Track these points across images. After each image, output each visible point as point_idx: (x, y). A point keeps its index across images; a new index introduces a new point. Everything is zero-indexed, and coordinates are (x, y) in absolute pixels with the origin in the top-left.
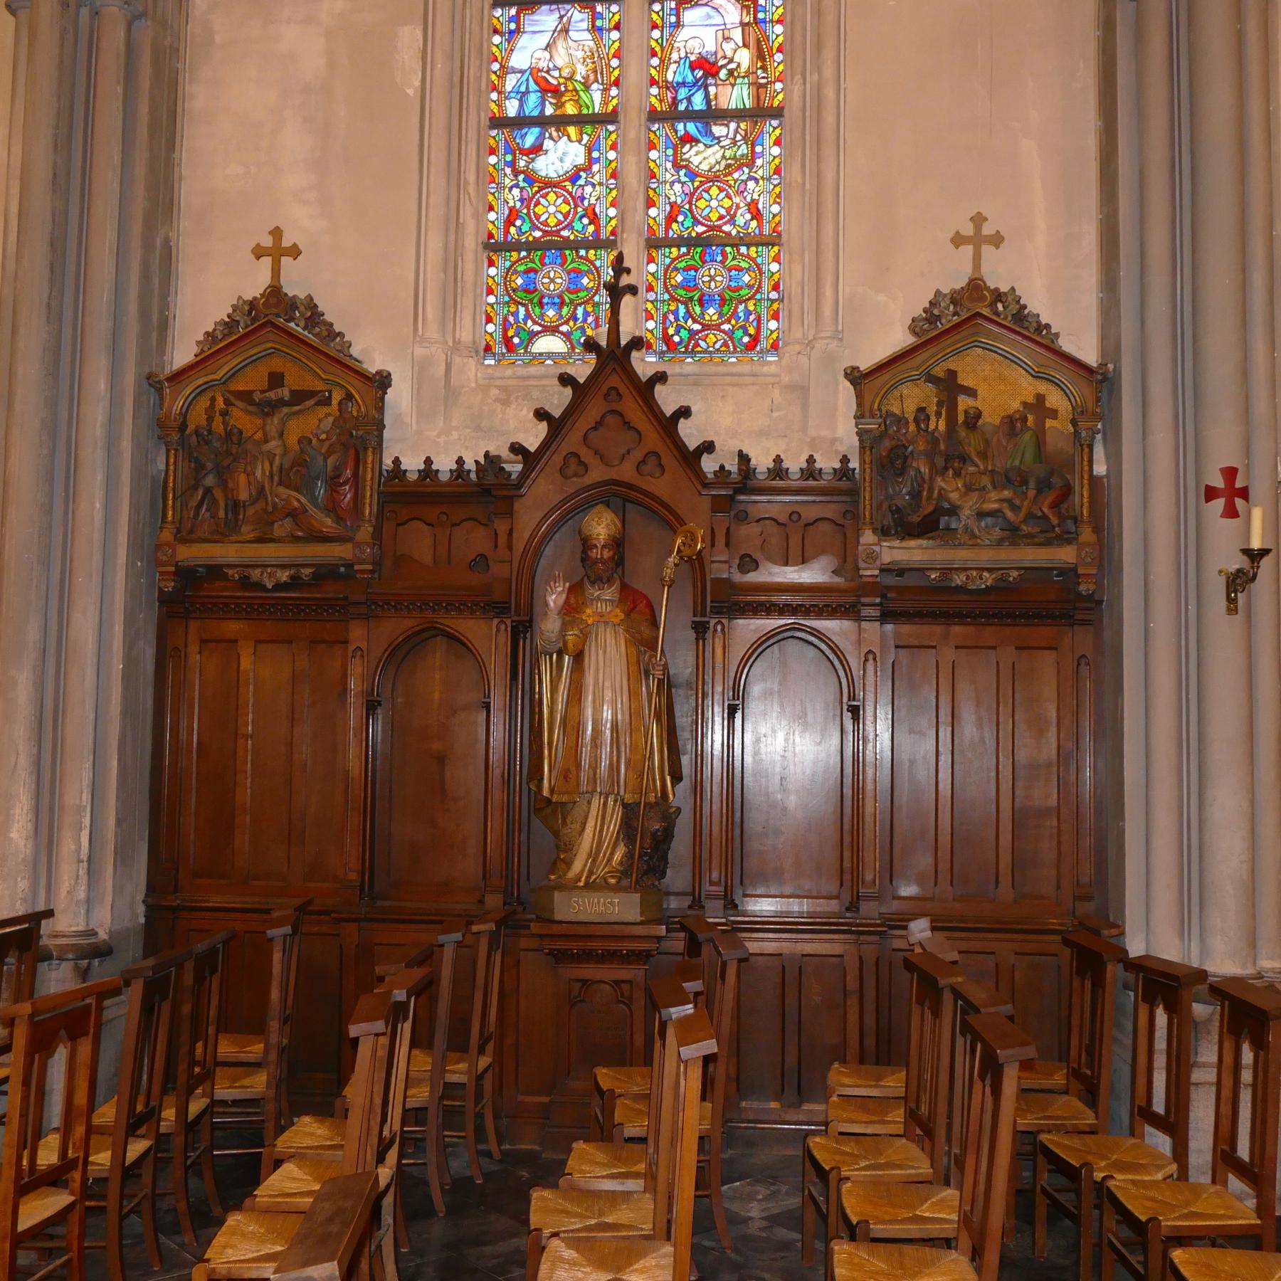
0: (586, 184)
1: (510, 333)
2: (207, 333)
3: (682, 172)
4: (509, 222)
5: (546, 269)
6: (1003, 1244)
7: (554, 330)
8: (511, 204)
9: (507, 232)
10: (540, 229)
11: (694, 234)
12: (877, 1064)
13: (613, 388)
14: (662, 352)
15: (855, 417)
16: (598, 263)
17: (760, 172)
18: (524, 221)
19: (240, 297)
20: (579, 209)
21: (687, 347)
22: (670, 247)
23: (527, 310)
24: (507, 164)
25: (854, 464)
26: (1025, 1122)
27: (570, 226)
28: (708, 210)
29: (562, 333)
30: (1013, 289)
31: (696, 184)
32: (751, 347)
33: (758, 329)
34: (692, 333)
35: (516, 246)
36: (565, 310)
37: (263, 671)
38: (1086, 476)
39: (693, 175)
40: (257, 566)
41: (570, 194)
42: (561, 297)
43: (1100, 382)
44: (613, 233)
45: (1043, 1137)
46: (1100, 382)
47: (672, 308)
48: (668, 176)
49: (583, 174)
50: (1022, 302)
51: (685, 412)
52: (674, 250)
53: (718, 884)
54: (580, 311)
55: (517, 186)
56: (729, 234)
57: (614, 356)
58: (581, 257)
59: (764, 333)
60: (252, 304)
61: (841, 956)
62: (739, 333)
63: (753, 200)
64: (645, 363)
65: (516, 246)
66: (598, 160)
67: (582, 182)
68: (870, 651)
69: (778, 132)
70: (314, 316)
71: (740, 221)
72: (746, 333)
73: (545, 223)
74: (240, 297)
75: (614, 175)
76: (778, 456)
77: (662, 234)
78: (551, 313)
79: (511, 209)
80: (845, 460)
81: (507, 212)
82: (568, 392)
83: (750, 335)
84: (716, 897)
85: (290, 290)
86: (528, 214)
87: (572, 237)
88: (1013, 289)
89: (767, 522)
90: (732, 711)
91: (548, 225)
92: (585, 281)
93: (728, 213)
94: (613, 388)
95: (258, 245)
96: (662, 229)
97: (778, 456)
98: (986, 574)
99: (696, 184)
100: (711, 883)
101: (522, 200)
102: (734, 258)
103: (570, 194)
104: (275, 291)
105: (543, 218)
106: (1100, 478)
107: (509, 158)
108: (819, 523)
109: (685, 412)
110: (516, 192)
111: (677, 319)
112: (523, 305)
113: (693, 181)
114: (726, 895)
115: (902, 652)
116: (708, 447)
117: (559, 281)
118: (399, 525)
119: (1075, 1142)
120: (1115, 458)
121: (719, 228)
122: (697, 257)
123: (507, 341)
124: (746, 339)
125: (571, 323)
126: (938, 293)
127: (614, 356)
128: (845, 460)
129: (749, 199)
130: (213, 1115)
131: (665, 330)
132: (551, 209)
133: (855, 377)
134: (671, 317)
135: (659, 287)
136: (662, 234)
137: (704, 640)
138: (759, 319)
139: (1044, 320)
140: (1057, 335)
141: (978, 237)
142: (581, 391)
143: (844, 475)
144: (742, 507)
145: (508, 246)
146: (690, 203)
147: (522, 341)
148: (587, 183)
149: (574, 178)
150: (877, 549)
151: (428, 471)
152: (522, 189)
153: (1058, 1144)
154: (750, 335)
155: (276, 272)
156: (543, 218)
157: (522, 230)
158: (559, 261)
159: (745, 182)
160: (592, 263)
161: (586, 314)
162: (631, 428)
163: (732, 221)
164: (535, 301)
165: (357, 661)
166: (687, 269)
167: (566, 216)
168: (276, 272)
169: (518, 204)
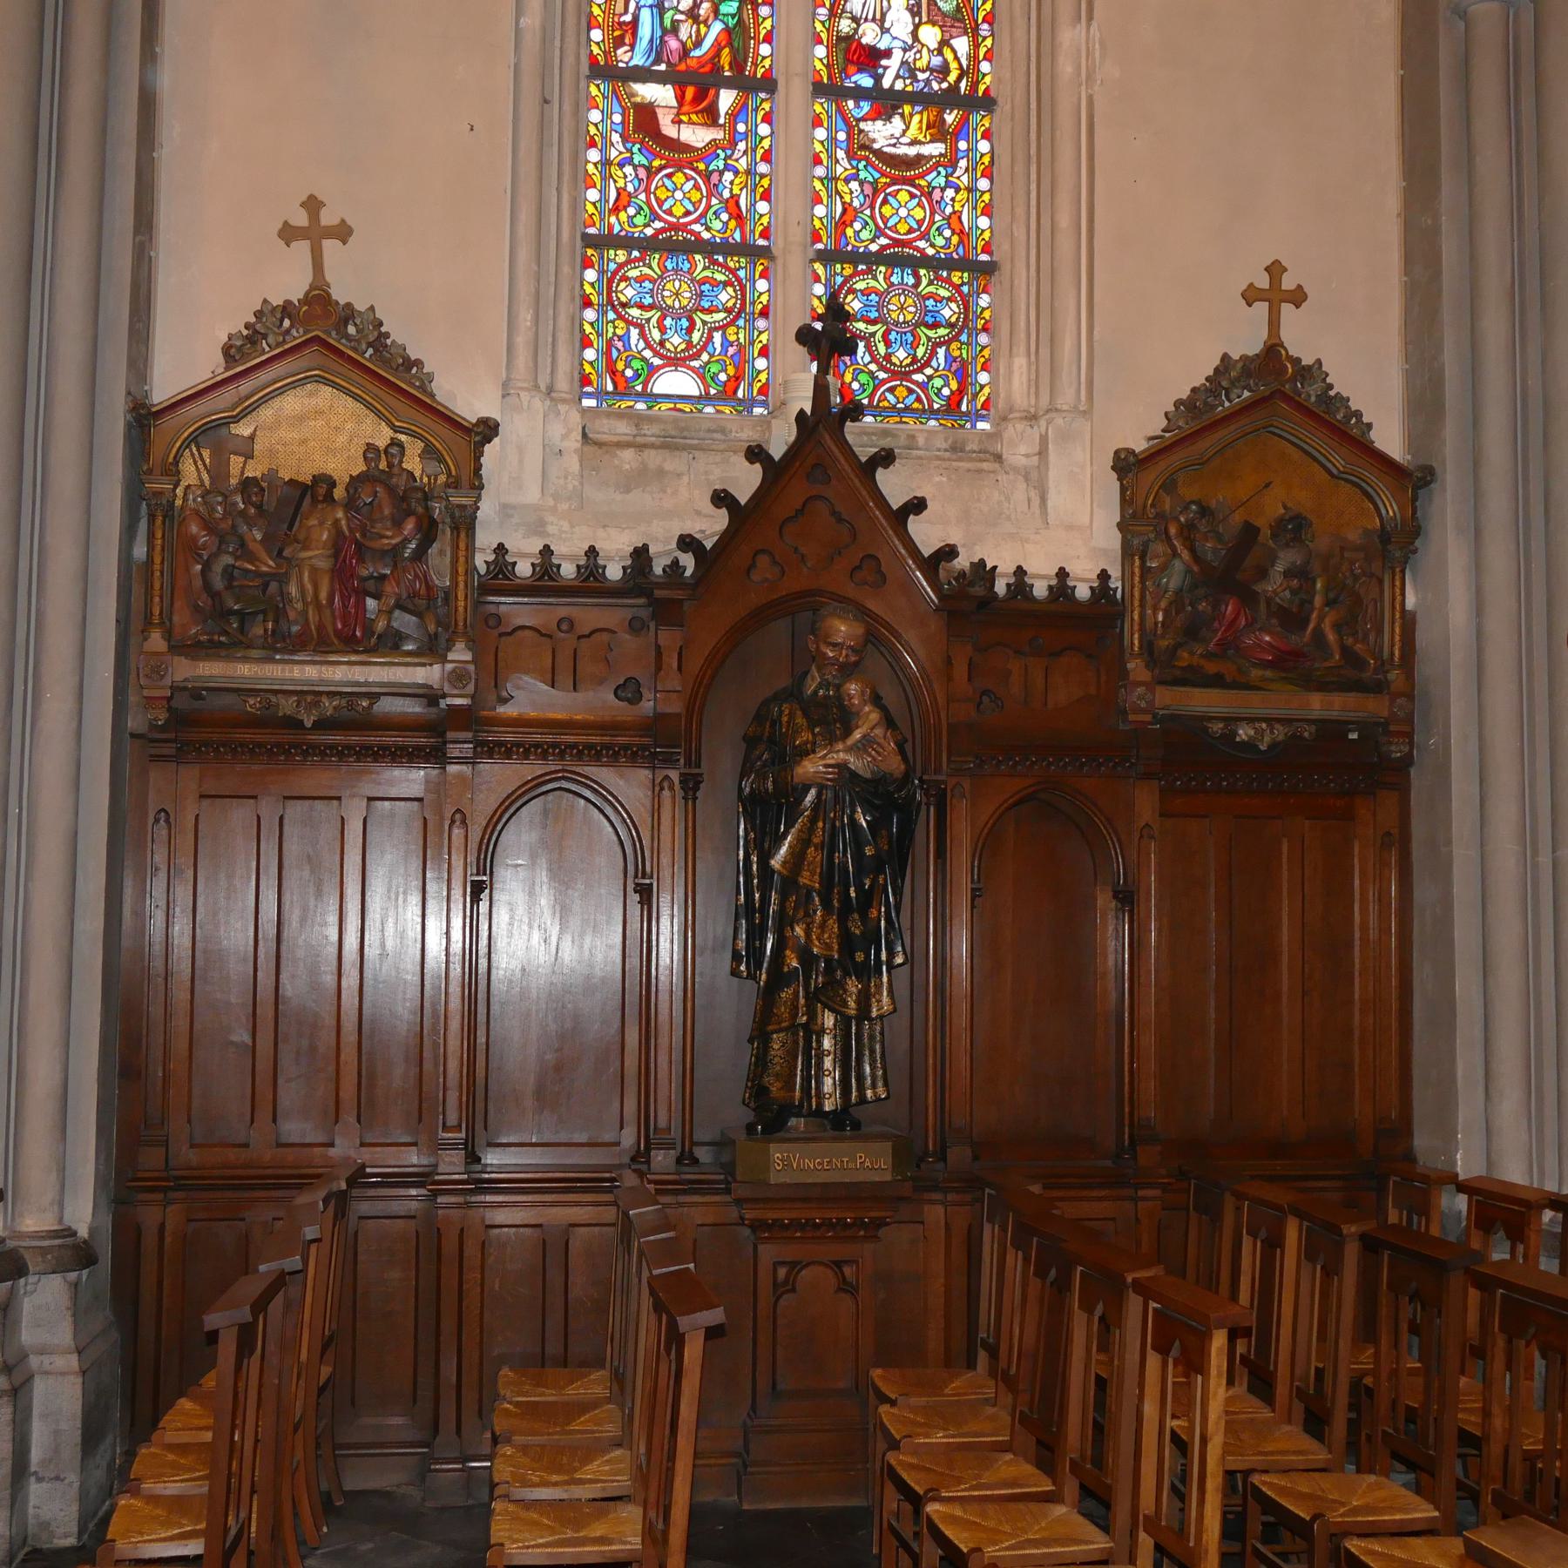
8: (621, 183)
20: (937, 218)
22: (616, 248)
25: (1115, 583)
26: (1235, 1463)
27: (925, 236)
29: (692, 369)
30: (372, 308)
35: (626, 242)
45: (1256, 1479)
51: (917, 506)
53: (458, 1128)
56: (922, 251)
60: (286, 309)
63: (732, 196)
68: (458, 811)
73: (894, 229)
78: (901, 354)
80: (1104, 576)
84: (453, 1146)
85: (340, 294)
86: (872, 217)
88: (1319, 362)
89: (527, 633)
90: (477, 890)
92: (947, 313)
98: (325, 700)
100: (445, 1128)
104: (1273, 350)
105: (691, 208)
108: (519, 633)
109: (917, 506)
114: (466, 1144)
115: (206, 802)
119: (1304, 1485)
121: (907, 244)
126: (1225, 357)
129: (726, 194)
133: (488, 430)
137: (695, 799)
139: (1354, 406)
140: (1369, 426)
142: (775, 472)
143: (591, 574)
144: (492, 609)
148: (727, 167)
150: (449, 666)
153: (1283, 1491)
155: (1274, 323)
156: (691, 208)
159: (721, 173)
161: (726, 343)
168: (1274, 323)
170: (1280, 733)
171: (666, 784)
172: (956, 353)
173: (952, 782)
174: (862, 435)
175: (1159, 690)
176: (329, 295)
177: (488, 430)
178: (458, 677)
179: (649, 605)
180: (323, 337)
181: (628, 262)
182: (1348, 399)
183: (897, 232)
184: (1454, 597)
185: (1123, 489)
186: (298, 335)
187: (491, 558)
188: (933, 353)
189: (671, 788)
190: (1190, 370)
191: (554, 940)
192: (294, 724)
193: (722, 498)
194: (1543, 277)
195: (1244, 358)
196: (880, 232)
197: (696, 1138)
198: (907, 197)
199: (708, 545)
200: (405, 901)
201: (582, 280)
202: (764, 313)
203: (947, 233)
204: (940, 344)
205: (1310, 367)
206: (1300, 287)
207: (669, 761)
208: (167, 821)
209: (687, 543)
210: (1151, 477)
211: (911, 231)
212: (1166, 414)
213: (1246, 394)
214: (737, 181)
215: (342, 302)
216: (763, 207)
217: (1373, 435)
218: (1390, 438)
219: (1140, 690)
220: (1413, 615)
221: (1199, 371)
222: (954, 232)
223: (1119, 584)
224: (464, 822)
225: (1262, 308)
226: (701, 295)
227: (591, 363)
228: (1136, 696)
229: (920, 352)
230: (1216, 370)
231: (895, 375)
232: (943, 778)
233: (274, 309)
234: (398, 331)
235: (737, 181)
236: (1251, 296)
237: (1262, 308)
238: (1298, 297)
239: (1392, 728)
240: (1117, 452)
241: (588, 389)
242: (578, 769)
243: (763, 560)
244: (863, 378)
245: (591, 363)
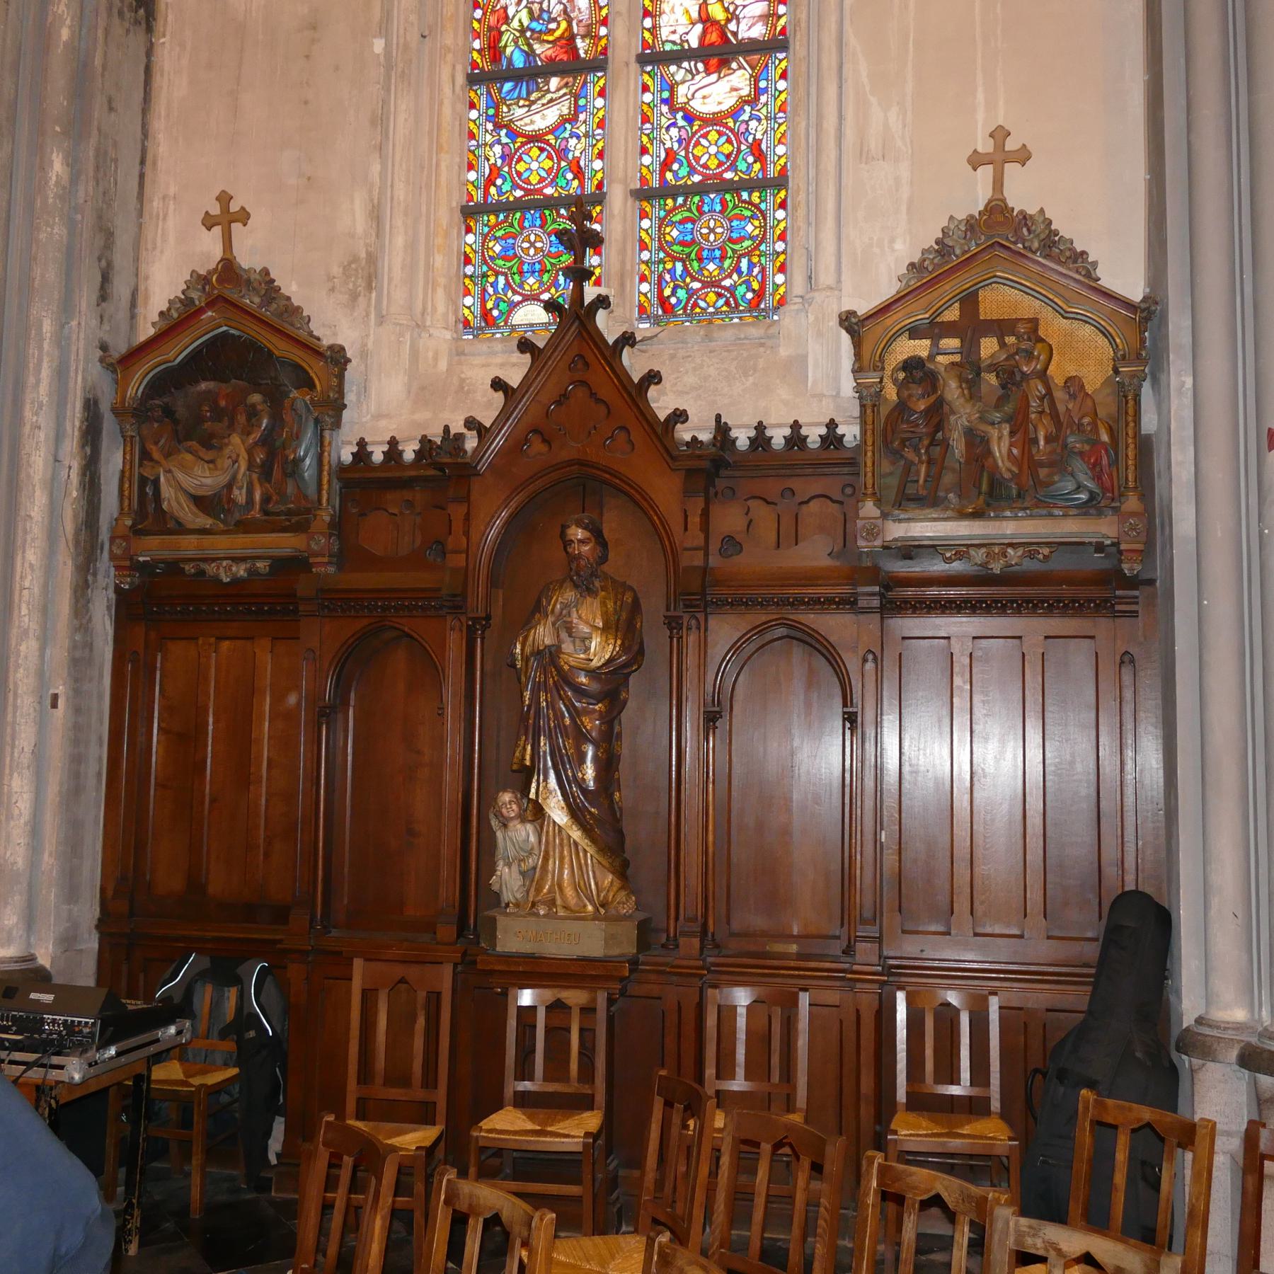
0: (751, 118)
1: (490, 305)
3: (503, 132)
4: (666, 166)
5: (706, 217)
6: (106, 1089)
7: (534, 298)
8: (668, 145)
9: (486, 193)
10: (522, 188)
11: (511, 199)
12: (351, 979)
13: (580, 361)
14: (480, 328)
15: (853, 371)
16: (763, 206)
17: (764, 111)
18: (505, 180)
19: (951, 218)
21: (685, 308)
23: (507, 279)
24: (664, 101)
28: (706, 156)
30: (1042, 211)
31: (695, 128)
32: (754, 305)
33: (763, 284)
34: (691, 293)
35: (495, 209)
36: (727, 263)
37: (279, 682)
39: (513, 134)
41: (732, 130)
42: (722, 249)
43: (1146, 316)
44: (600, 186)
46: (1146, 316)
47: (669, 266)
48: (664, 120)
49: (748, 108)
52: (492, 218)
54: (744, 264)
55: (674, 124)
57: (576, 318)
58: (744, 202)
59: (769, 288)
60: (972, 225)
62: (741, 290)
65: (495, 209)
66: (766, 90)
67: (745, 117)
69: (602, 82)
71: (742, 166)
72: (750, 289)
73: (705, 166)
74: (951, 218)
75: (601, 125)
77: (656, 184)
79: (669, 152)
81: (663, 155)
82: (527, 358)
83: (754, 291)
86: (509, 173)
87: (736, 178)
91: (530, 183)
92: (749, 228)
93: (549, 175)
94: (580, 361)
96: (656, 177)
98: (1010, 551)
99: (695, 128)
101: (503, 157)
102: (554, 221)
103: (732, 130)
104: (997, 210)
107: (491, 112)
110: (674, 132)
111: (496, 291)
112: (503, 274)
113: (514, 142)
117: (719, 230)
118: (801, 503)
121: (539, 191)
122: (694, 208)
123: (486, 314)
124: (750, 295)
125: (735, 276)
127: (576, 318)
129: (750, 139)
131: (660, 291)
132: (535, 165)
134: (667, 277)
135: (476, 259)
136: (656, 184)
138: (763, 270)
140: (1095, 264)
145: (667, 191)
146: (686, 149)
147: (679, 301)
149: (735, 113)
152: (504, 145)
154: (754, 291)
155: (998, 183)
156: (702, 162)
157: (505, 190)
158: (538, 222)
160: (757, 206)
161: (751, 266)
163: (734, 167)
164: (515, 269)
167: (549, 171)
168: (998, 183)
169: (676, 146)
176: (1004, 200)
177: (850, 322)
181: (675, 208)
184: (1187, 416)
191: (508, 843)
193: (498, 384)
194: (1250, 91)
196: (693, 171)
202: (782, 237)
214: (760, 128)
216: (598, 164)
220: (1148, 438)
225: (986, 172)
226: (731, 229)
235: (760, 128)
237: (986, 172)
240: (840, 316)
242: (791, 617)
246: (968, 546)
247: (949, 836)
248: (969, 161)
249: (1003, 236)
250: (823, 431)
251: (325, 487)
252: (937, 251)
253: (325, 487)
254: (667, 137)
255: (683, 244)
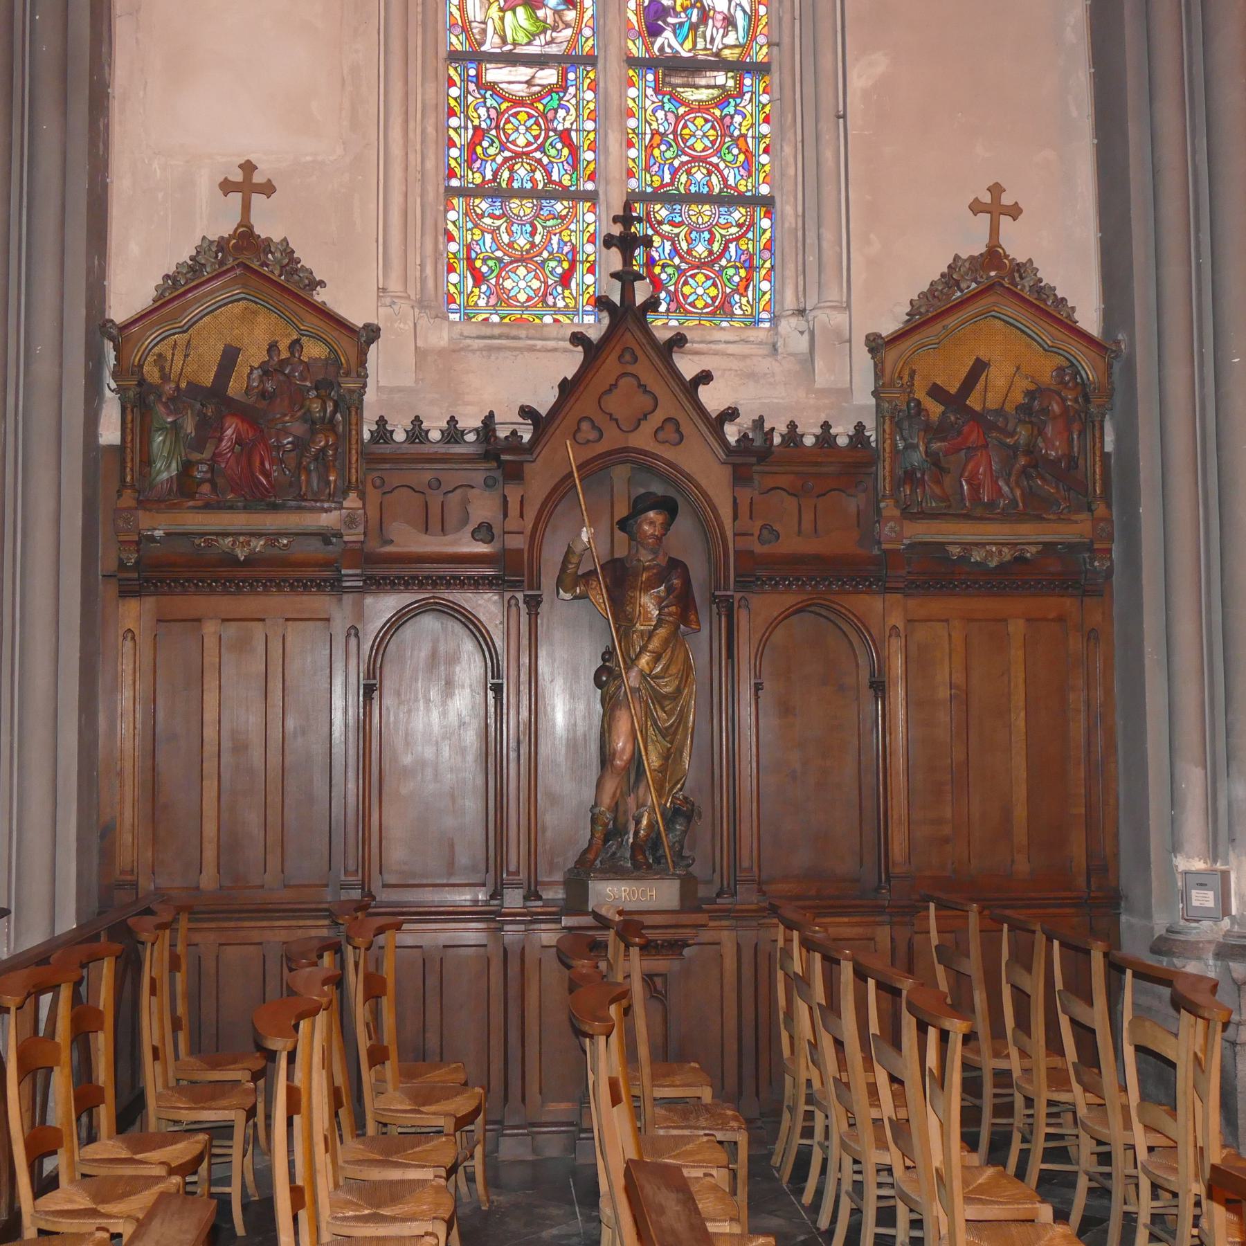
2: (167, 277)
13: (627, 345)
25: (871, 433)
30: (1030, 260)
38: (1098, 453)
40: (226, 535)
50: (1039, 275)
60: (222, 245)
61: (485, 946)
64: (663, 324)
70: (290, 261)
74: (204, 238)
76: (382, 418)
80: (860, 427)
85: (262, 230)
88: (1030, 260)
94: (627, 345)
95: (976, 199)
97: (382, 418)
104: (993, 256)
106: (1108, 454)
114: (363, 884)
116: (731, 414)
120: (1127, 435)
126: (957, 258)
127: (626, 316)
128: (860, 427)
130: (212, 1146)
133: (372, 333)
140: (1073, 308)
141: (995, 208)
151: (826, 437)
155: (994, 230)
162: (646, 391)
165: (894, 641)
166: (728, 226)
168: (994, 230)
170: (1007, 554)
171: (513, 602)
172: (744, 247)
173: (738, 596)
174: (663, 324)
175: (906, 522)
176: (251, 228)
177: (372, 333)
178: (350, 522)
179: (499, 467)
180: (249, 265)
182: (1054, 289)
183: (694, 150)
185: (876, 365)
186: (230, 262)
187: (375, 427)
188: (726, 248)
189: (517, 605)
190: (929, 267)
192: (232, 561)
195: (972, 258)
197: (539, 879)
198: (702, 122)
199: (544, 412)
200: (803, 908)
201: (446, 219)
203: (735, 151)
204: (731, 241)
205: (1024, 265)
206: (269, 180)
207: (516, 586)
208: (133, 638)
209: (527, 412)
210: (891, 356)
211: (693, 276)
212: (911, 302)
213: (974, 285)
215: (263, 236)
217: (1076, 316)
218: (1089, 318)
219: (892, 524)
221: (936, 267)
222: (740, 150)
223: (874, 433)
224: (357, 635)
227: (455, 285)
228: (887, 529)
229: (716, 247)
230: (949, 267)
231: (703, 160)
232: (729, 593)
233: (211, 242)
234: (309, 258)
236: (227, 187)
237: (236, 198)
238: (1015, 212)
239: (1096, 546)
240: (867, 337)
241: (453, 306)
243: (585, 426)
244: (670, 270)
245: (455, 285)
246: (217, 534)
247: (327, 729)
248: (1021, 211)
249: (990, 284)
250: (818, 431)
251: (129, 426)
252: (189, 266)
253: (129, 426)
254: (475, 115)
255: (711, 241)
